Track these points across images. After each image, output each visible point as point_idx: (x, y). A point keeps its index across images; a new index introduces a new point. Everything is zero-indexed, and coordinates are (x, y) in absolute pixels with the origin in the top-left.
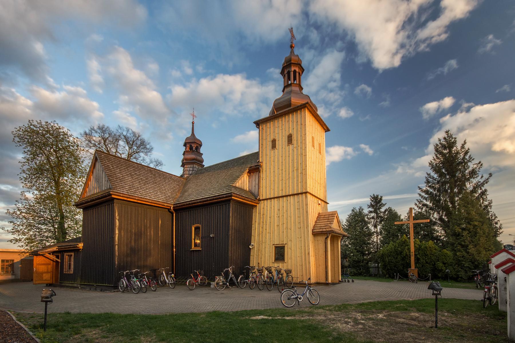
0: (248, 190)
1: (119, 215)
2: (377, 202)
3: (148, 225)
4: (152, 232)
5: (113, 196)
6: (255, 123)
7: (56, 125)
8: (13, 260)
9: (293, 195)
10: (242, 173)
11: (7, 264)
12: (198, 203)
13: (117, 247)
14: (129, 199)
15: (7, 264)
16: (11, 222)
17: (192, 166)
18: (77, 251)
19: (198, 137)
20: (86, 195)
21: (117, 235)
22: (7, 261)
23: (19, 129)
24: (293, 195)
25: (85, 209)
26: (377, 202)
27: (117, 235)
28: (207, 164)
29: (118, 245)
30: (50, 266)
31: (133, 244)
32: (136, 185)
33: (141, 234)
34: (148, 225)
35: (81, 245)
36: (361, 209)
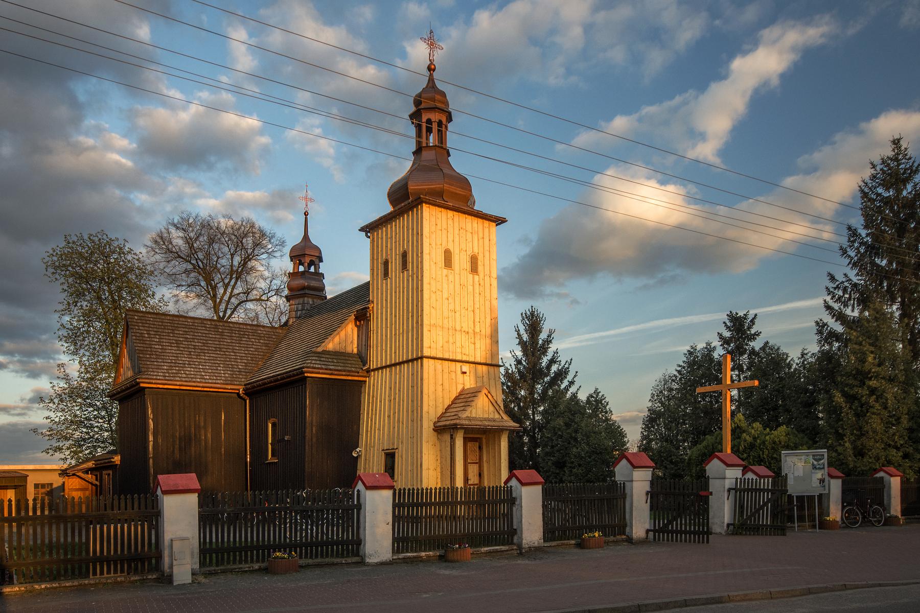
0: (355, 351)
1: (153, 412)
2: (740, 328)
3: (202, 424)
4: (209, 435)
5: (142, 385)
6: (362, 230)
7: (105, 237)
8: (51, 484)
9: (407, 362)
10: (342, 321)
11: (43, 490)
12: (294, 375)
13: (151, 461)
14: (166, 387)
15: (43, 490)
16: (47, 418)
17: (301, 300)
18: (113, 467)
19: (314, 240)
20: (121, 379)
21: (151, 443)
22: (43, 486)
23: (51, 252)
24: (407, 362)
25: (121, 401)
26: (740, 328)
27: (151, 443)
28: (332, 290)
29: (272, 444)
30: (87, 493)
31: (177, 455)
32: (185, 359)
33: (190, 440)
34: (202, 424)
35: (117, 459)
36: (710, 349)
